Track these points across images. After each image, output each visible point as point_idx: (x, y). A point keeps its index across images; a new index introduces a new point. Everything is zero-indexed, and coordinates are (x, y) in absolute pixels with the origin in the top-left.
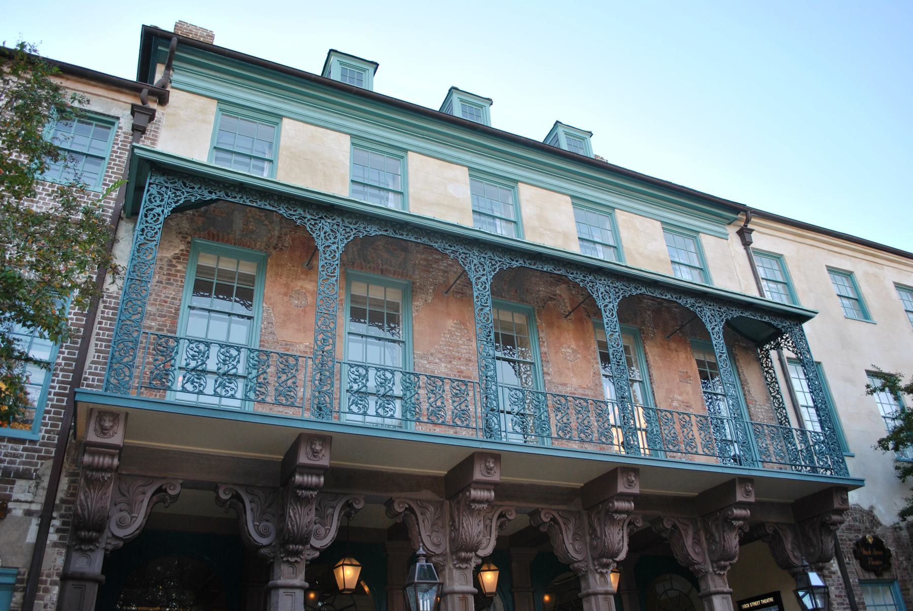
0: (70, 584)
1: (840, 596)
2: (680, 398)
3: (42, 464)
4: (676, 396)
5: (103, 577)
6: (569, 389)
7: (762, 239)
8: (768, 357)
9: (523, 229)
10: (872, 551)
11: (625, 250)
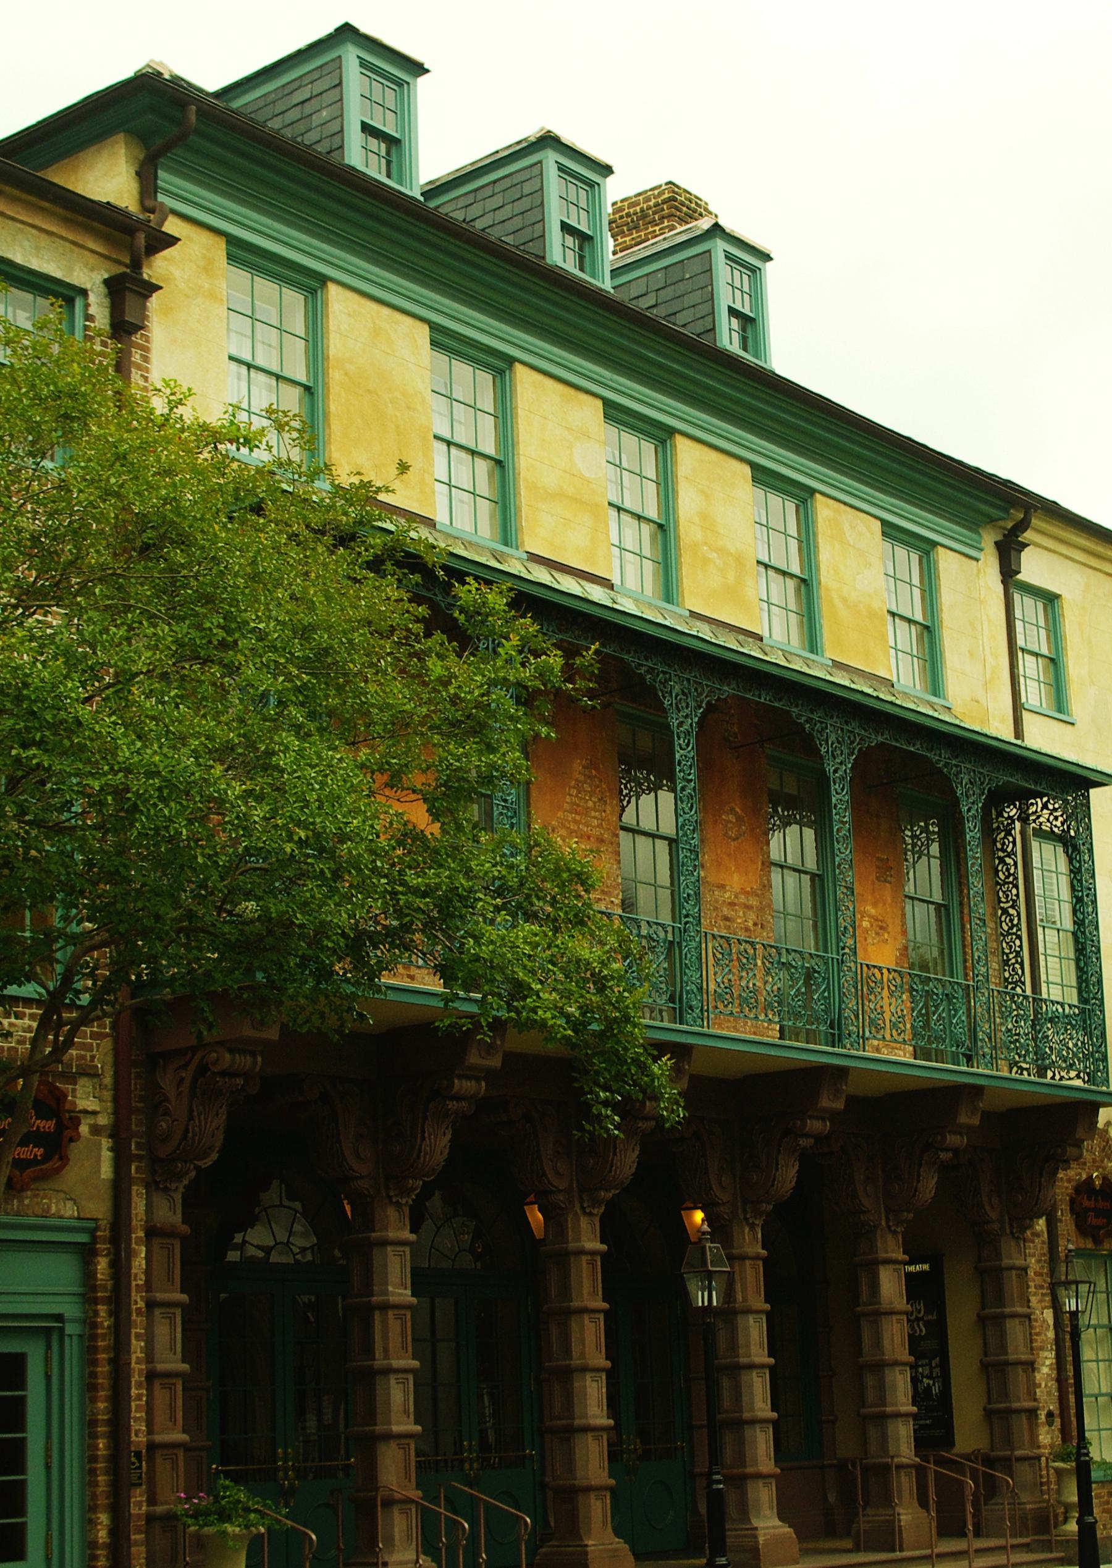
0: (156, 1241)
1: (1041, 1275)
2: (873, 911)
3: (98, 1045)
4: (868, 908)
5: (185, 1229)
6: (727, 895)
7: (1035, 567)
8: (1008, 833)
9: (678, 548)
10: (1096, 1200)
11: (823, 593)
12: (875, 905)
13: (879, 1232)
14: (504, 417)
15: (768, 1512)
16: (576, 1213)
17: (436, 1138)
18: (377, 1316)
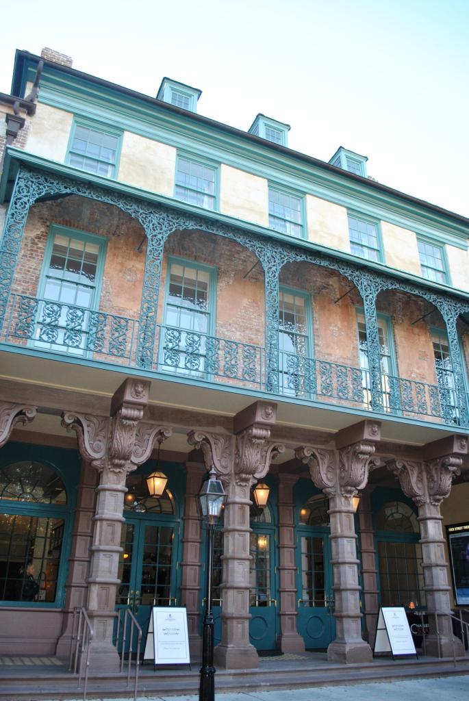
2: (418, 371)
6: (333, 358)
11: (386, 253)
12: (418, 368)
13: (426, 506)
14: (444, 259)
15: (355, 635)
16: (233, 485)
17: (252, 456)
18: (99, 523)
